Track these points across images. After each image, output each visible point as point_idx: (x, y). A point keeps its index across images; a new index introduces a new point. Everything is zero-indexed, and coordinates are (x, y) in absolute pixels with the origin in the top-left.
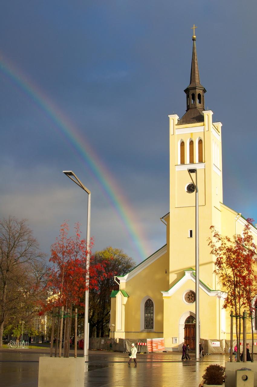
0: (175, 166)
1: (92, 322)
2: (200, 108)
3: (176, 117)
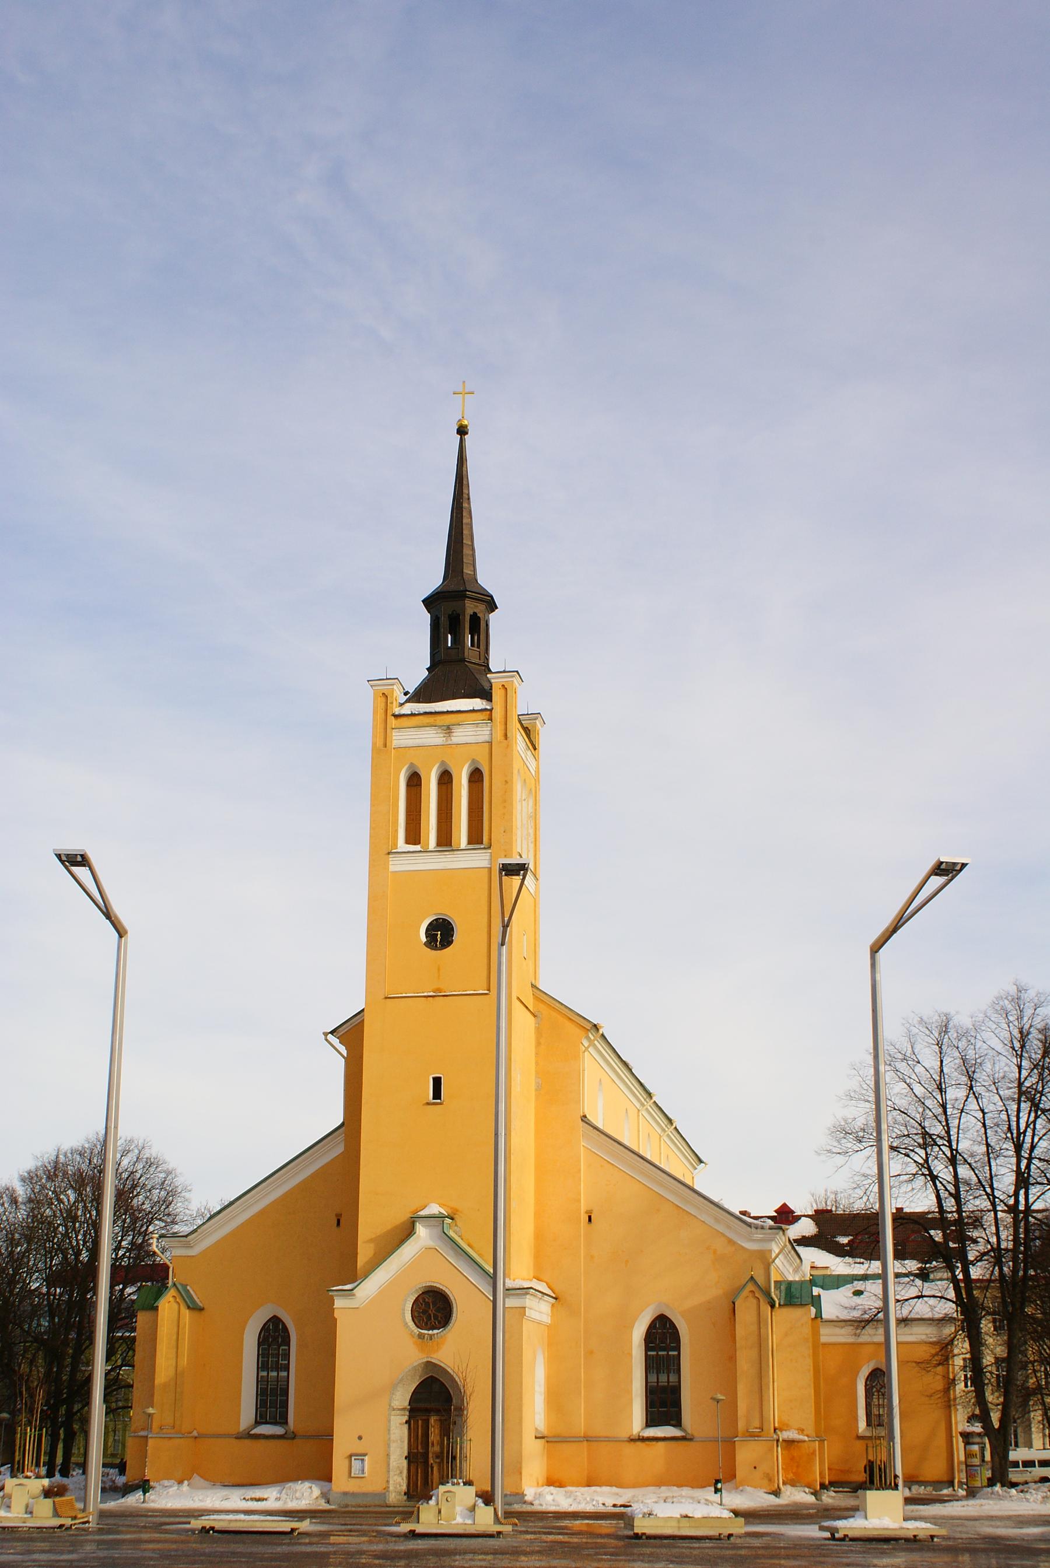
0: (462, 431)
1: (63, 1410)
2: (477, 661)
3: (395, 687)
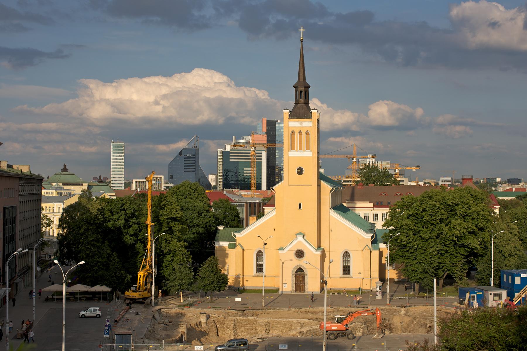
0: (302, 41)
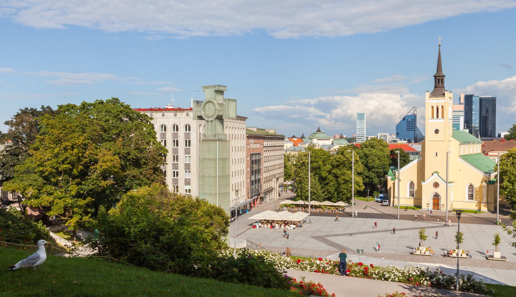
0: (439, 46)
